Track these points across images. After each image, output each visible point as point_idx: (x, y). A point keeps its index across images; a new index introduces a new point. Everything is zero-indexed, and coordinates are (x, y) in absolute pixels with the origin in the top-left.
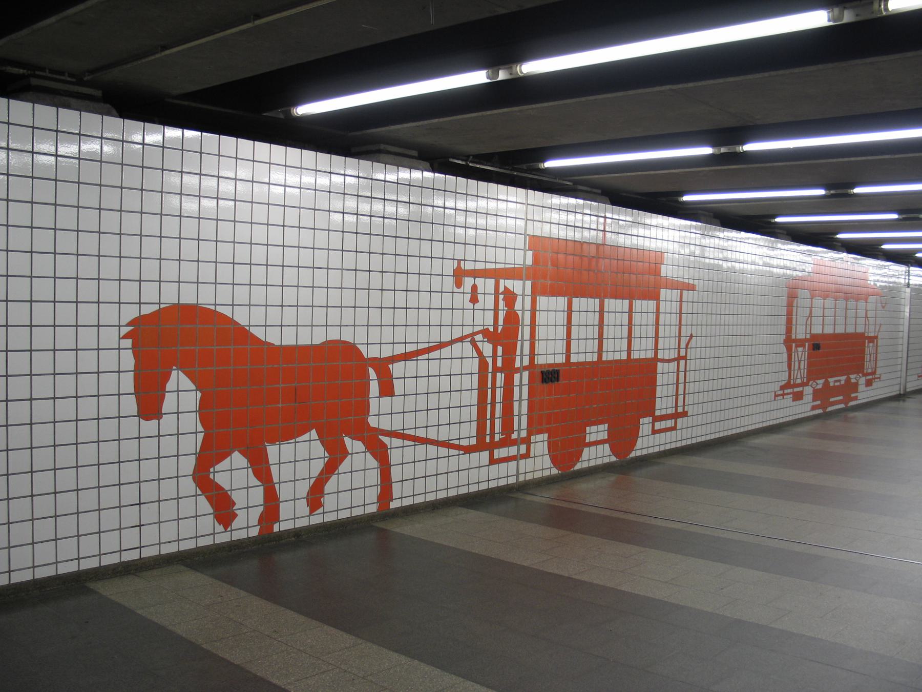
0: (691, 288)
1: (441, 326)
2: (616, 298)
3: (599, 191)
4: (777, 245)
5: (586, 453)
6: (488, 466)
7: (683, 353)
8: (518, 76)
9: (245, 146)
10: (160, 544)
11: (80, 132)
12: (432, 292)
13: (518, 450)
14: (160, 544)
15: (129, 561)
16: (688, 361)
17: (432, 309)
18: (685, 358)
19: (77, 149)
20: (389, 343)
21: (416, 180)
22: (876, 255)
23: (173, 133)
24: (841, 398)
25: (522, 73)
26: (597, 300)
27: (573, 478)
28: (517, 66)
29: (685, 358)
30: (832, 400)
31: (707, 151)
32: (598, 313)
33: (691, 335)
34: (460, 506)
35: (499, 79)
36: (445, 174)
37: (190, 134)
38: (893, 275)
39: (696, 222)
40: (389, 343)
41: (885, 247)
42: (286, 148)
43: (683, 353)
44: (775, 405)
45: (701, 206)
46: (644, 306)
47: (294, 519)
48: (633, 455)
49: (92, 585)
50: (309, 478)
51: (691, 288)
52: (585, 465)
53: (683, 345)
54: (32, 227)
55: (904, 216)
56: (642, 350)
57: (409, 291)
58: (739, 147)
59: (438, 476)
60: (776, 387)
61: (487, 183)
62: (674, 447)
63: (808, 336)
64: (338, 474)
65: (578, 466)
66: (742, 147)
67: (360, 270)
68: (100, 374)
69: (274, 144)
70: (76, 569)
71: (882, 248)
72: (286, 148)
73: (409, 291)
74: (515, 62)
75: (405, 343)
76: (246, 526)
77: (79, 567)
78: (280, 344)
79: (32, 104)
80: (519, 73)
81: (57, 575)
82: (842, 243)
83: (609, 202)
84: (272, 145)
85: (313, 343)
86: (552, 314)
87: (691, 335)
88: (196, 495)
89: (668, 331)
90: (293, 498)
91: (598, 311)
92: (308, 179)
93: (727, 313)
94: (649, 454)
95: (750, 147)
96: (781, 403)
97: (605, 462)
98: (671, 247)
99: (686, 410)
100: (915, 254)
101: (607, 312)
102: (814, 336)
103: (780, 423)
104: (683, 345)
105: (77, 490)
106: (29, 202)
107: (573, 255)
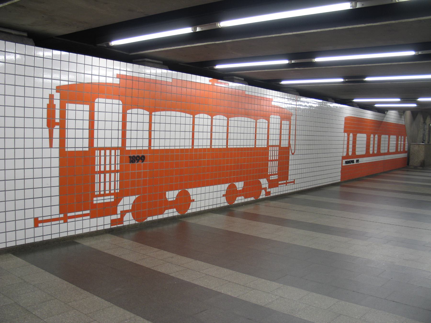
1: (137, 139)
4: (300, 99)
5: (193, 205)
6: (34, 228)
8: (218, 28)
10: (25, 239)
11: (15, 52)
14: (25, 239)
17: (179, 131)
19: (6, 57)
20: (163, 146)
22: (145, 61)
23: (57, 53)
25: (220, 26)
28: (218, 23)
31: (286, 62)
32: (267, 135)
35: (197, 31)
37: (63, 53)
38: (301, 105)
39: (243, 84)
40: (163, 146)
41: (376, 105)
45: (294, 86)
47: (67, 231)
49: (78, 241)
54: (43, 98)
62: (275, 195)
65: (189, 211)
68: (43, 159)
71: (354, 101)
76: (52, 235)
77: (60, 236)
78: (111, 146)
79: (4, 41)
80: (219, 26)
81: (16, 245)
82: (163, 62)
83: (248, 84)
84: (134, 64)
86: (235, 134)
88: (168, 199)
90: (60, 224)
91: (267, 133)
95: (224, 24)
100: (353, 100)
101: (191, 132)
103: (329, 184)
105: (34, 208)
106: (35, 87)
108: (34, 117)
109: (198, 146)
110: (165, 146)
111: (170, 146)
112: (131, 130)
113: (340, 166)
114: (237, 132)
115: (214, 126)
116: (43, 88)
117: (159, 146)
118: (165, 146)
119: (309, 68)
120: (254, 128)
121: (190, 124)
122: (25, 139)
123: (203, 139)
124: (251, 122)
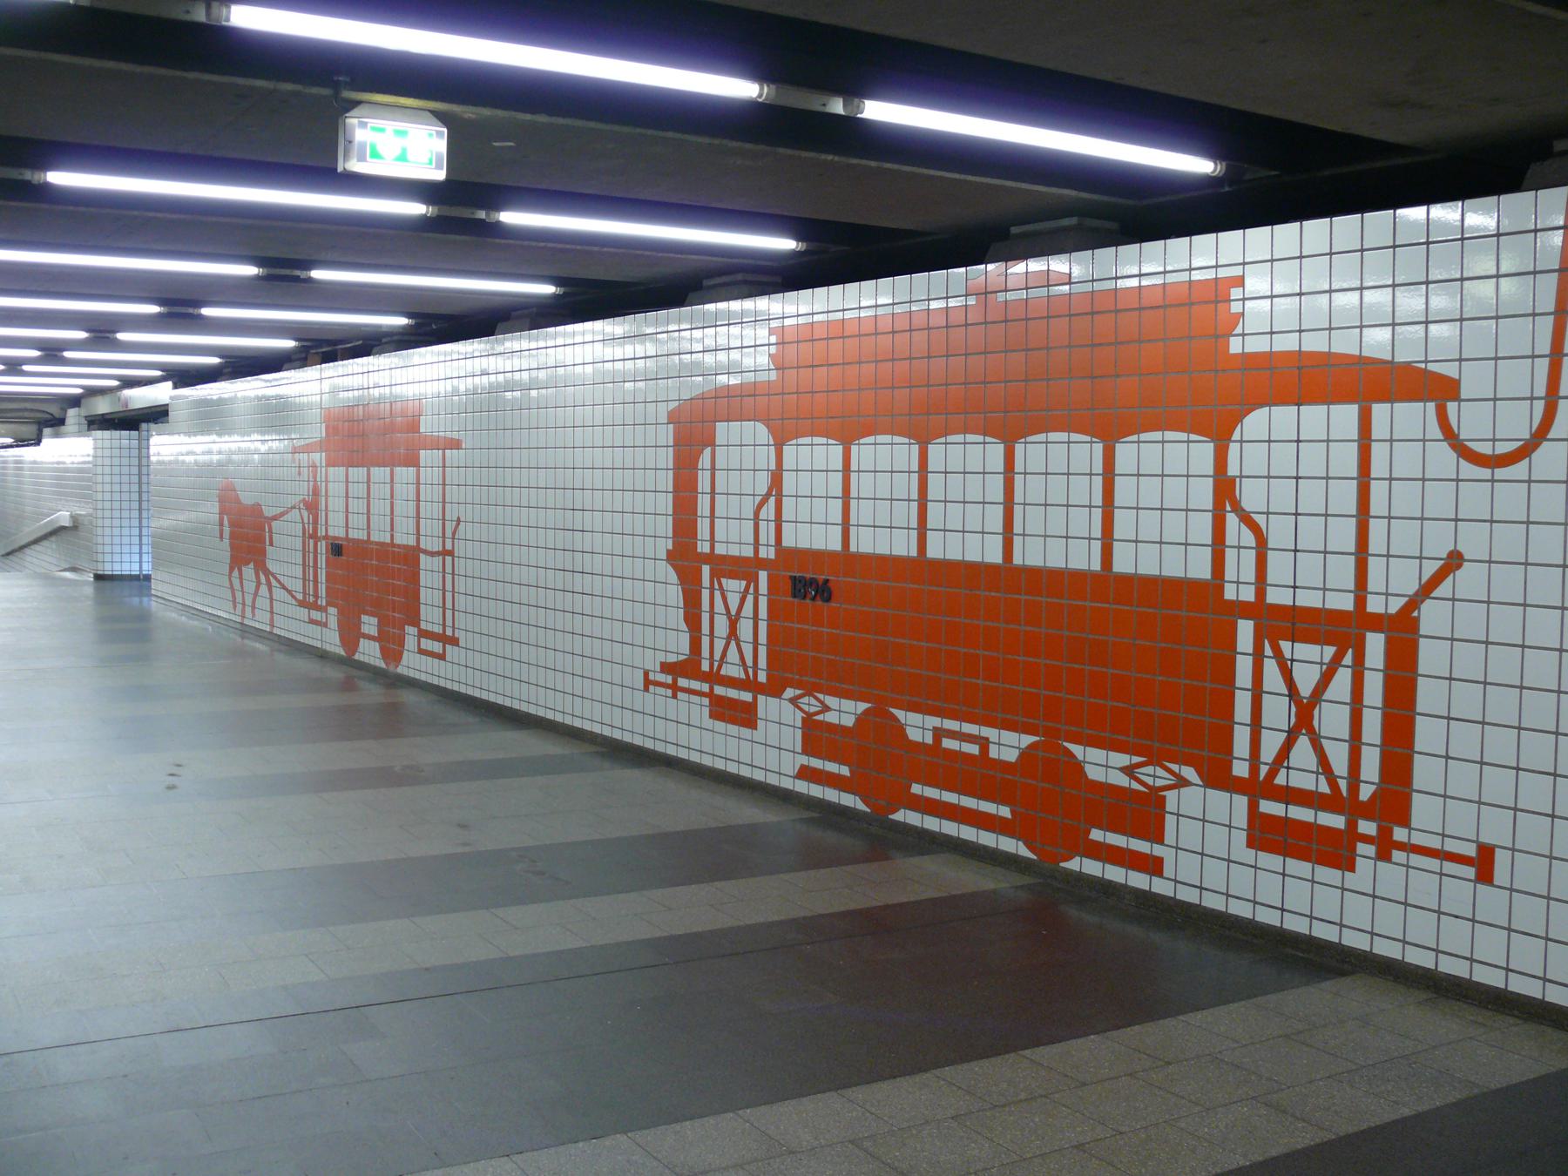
0: (455, 444)
1: (1047, 474)
2: (334, 466)
7: (448, 546)
13: (1367, 839)
16: (456, 559)
18: (451, 553)
24: (845, 771)
26: (365, 469)
27: (321, 657)
29: (451, 553)
30: (1096, 835)
33: (459, 518)
43: (448, 546)
44: (640, 699)
46: (405, 473)
51: (455, 444)
53: (449, 533)
55: (191, 310)
56: (404, 538)
57: (1274, 441)
60: (652, 662)
63: (768, 553)
73: (1274, 441)
87: (459, 518)
89: (430, 510)
93: (356, 484)
96: (659, 700)
98: (430, 389)
99: (1470, 850)
102: (786, 556)
104: (449, 533)
108: (1388, 560)
109: (1163, 442)
110: (965, 443)
111: (965, 443)
112: (1046, 505)
113: (298, 608)
114: (665, 490)
115: (1386, 609)
116: (1485, 683)
117: (1494, 440)
118: (1047, 442)
119: (124, 66)
120: (666, 515)
121: (858, 526)
122: (1421, 477)
123: (812, 471)
124: (644, 536)
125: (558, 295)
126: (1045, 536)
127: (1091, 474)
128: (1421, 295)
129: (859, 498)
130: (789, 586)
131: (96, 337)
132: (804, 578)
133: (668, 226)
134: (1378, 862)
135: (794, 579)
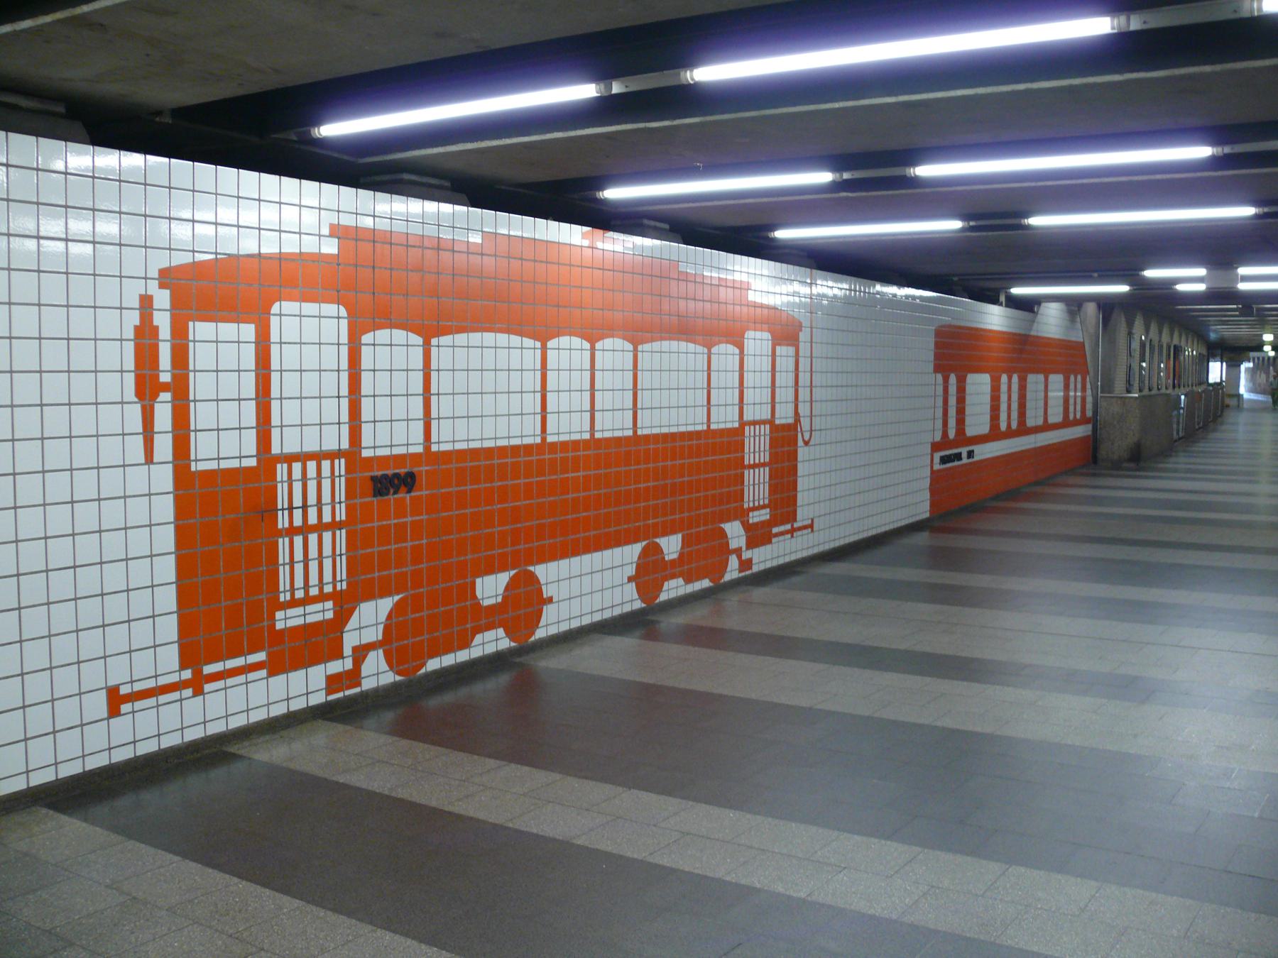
3: (61, 109)
9: (228, 174)
12: (92, 372)
15: (295, 711)
21: (134, 170)
22: (401, 181)
34: (298, 725)
36: (169, 156)
42: (280, 178)
48: (657, 601)
49: (233, 749)
50: (496, 596)
52: (553, 630)
58: (686, 72)
59: (29, 742)
61: (278, 177)
64: (677, 552)
65: (540, 634)
66: (692, 71)
67: (396, 345)
69: (307, 179)
70: (53, 778)
71: (1144, 276)
72: (280, 178)
74: (688, 67)
75: (124, 466)
85: (303, 450)
92: (249, 216)
94: (606, 620)
95: (708, 73)
97: (625, 611)
107: (711, 301)
125: (771, 231)
126: (124, 435)
127: (122, 371)
128: (116, 223)
129: (642, 390)
130: (370, 484)
131: (1136, 270)
132: (387, 475)
133: (723, 179)
134: (105, 690)
135: (373, 479)
